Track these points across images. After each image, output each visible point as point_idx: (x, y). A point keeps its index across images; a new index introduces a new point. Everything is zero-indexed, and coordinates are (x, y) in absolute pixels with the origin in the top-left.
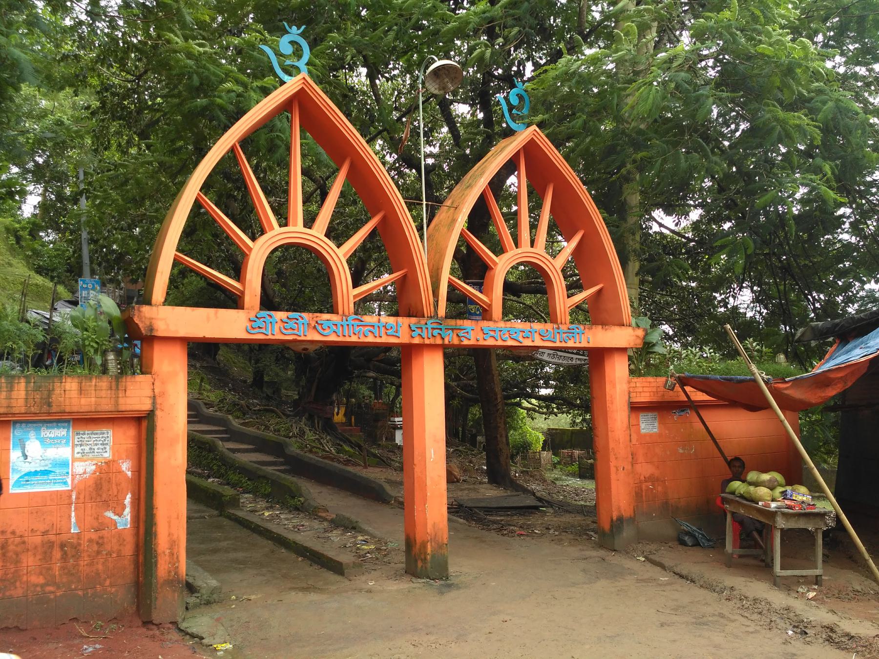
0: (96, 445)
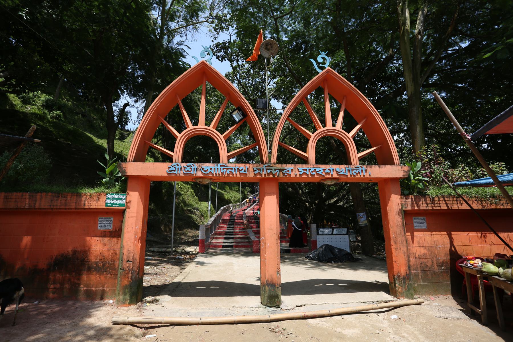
0: (107, 223)
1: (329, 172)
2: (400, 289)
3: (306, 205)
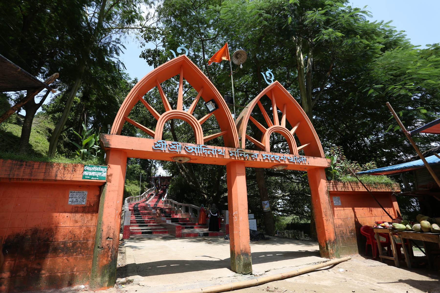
0: (79, 198)
1: (283, 159)
2: (331, 251)
3: (205, 197)
